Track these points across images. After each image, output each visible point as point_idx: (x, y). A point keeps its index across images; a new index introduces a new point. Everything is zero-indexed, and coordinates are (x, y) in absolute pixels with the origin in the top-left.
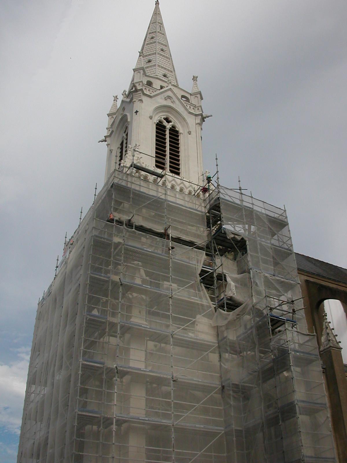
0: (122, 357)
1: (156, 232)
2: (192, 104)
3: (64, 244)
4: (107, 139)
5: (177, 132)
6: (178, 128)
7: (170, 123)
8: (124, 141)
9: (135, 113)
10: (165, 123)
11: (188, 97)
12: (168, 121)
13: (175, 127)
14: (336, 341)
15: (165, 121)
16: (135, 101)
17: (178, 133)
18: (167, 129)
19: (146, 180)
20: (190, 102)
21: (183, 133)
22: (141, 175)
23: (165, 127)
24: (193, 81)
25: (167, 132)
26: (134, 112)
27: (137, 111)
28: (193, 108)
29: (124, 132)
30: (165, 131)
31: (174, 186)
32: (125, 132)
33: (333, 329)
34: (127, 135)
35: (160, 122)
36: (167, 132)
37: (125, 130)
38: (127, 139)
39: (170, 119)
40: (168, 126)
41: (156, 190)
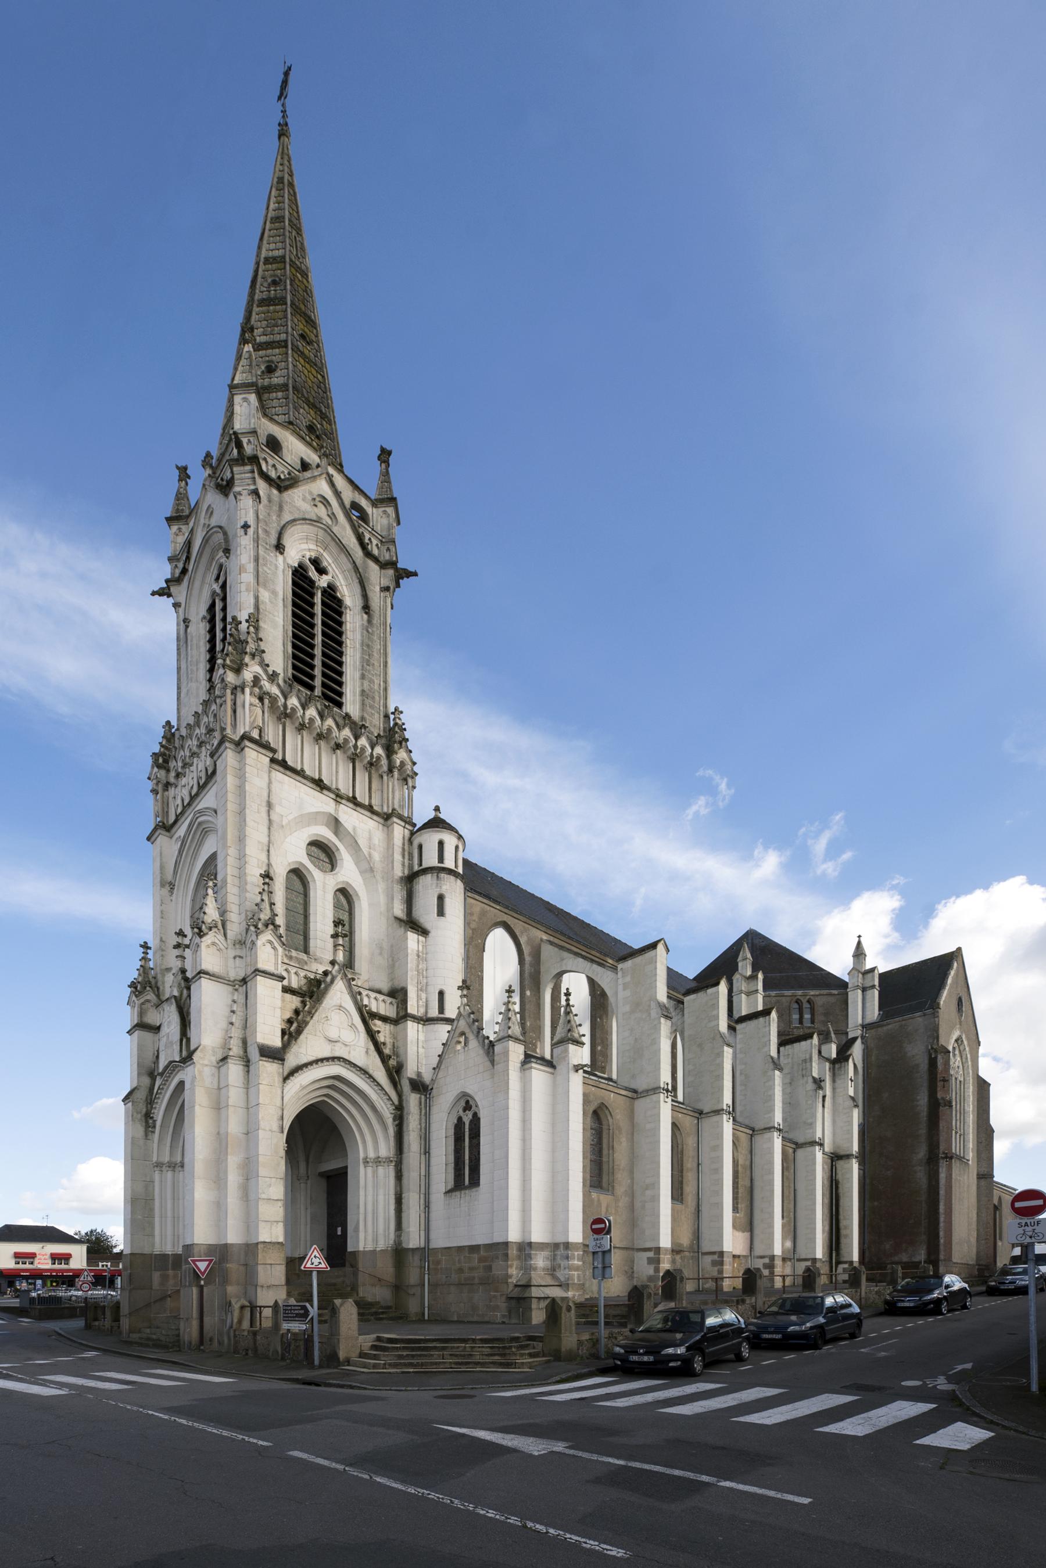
0: (289, 316)
1: (360, 1113)
2: (374, 533)
3: (151, 796)
4: (173, 589)
5: (339, 602)
6: (340, 593)
7: (324, 577)
8: (217, 601)
9: (243, 530)
10: (313, 573)
11: (367, 511)
12: (322, 571)
13: (336, 588)
14: (579, 1033)
15: (313, 568)
16: (240, 494)
17: (341, 607)
18: (318, 588)
19: (959, 1265)
20: (371, 525)
21: (351, 608)
22: (264, 693)
23: (312, 583)
24: (379, 462)
25: (318, 599)
26: (239, 526)
27: (246, 522)
28: (377, 545)
29: (214, 577)
30: (312, 595)
31: (331, 730)
32: (217, 579)
33: (576, 1015)
34: (224, 587)
35: (301, 566)
36: (318, 599)
37: (216, 572)
38: (224, 599)
39: (325, 564)
40: (323, 581)
41: (786, 1284)
